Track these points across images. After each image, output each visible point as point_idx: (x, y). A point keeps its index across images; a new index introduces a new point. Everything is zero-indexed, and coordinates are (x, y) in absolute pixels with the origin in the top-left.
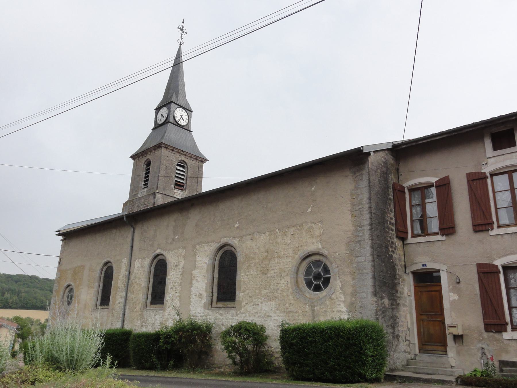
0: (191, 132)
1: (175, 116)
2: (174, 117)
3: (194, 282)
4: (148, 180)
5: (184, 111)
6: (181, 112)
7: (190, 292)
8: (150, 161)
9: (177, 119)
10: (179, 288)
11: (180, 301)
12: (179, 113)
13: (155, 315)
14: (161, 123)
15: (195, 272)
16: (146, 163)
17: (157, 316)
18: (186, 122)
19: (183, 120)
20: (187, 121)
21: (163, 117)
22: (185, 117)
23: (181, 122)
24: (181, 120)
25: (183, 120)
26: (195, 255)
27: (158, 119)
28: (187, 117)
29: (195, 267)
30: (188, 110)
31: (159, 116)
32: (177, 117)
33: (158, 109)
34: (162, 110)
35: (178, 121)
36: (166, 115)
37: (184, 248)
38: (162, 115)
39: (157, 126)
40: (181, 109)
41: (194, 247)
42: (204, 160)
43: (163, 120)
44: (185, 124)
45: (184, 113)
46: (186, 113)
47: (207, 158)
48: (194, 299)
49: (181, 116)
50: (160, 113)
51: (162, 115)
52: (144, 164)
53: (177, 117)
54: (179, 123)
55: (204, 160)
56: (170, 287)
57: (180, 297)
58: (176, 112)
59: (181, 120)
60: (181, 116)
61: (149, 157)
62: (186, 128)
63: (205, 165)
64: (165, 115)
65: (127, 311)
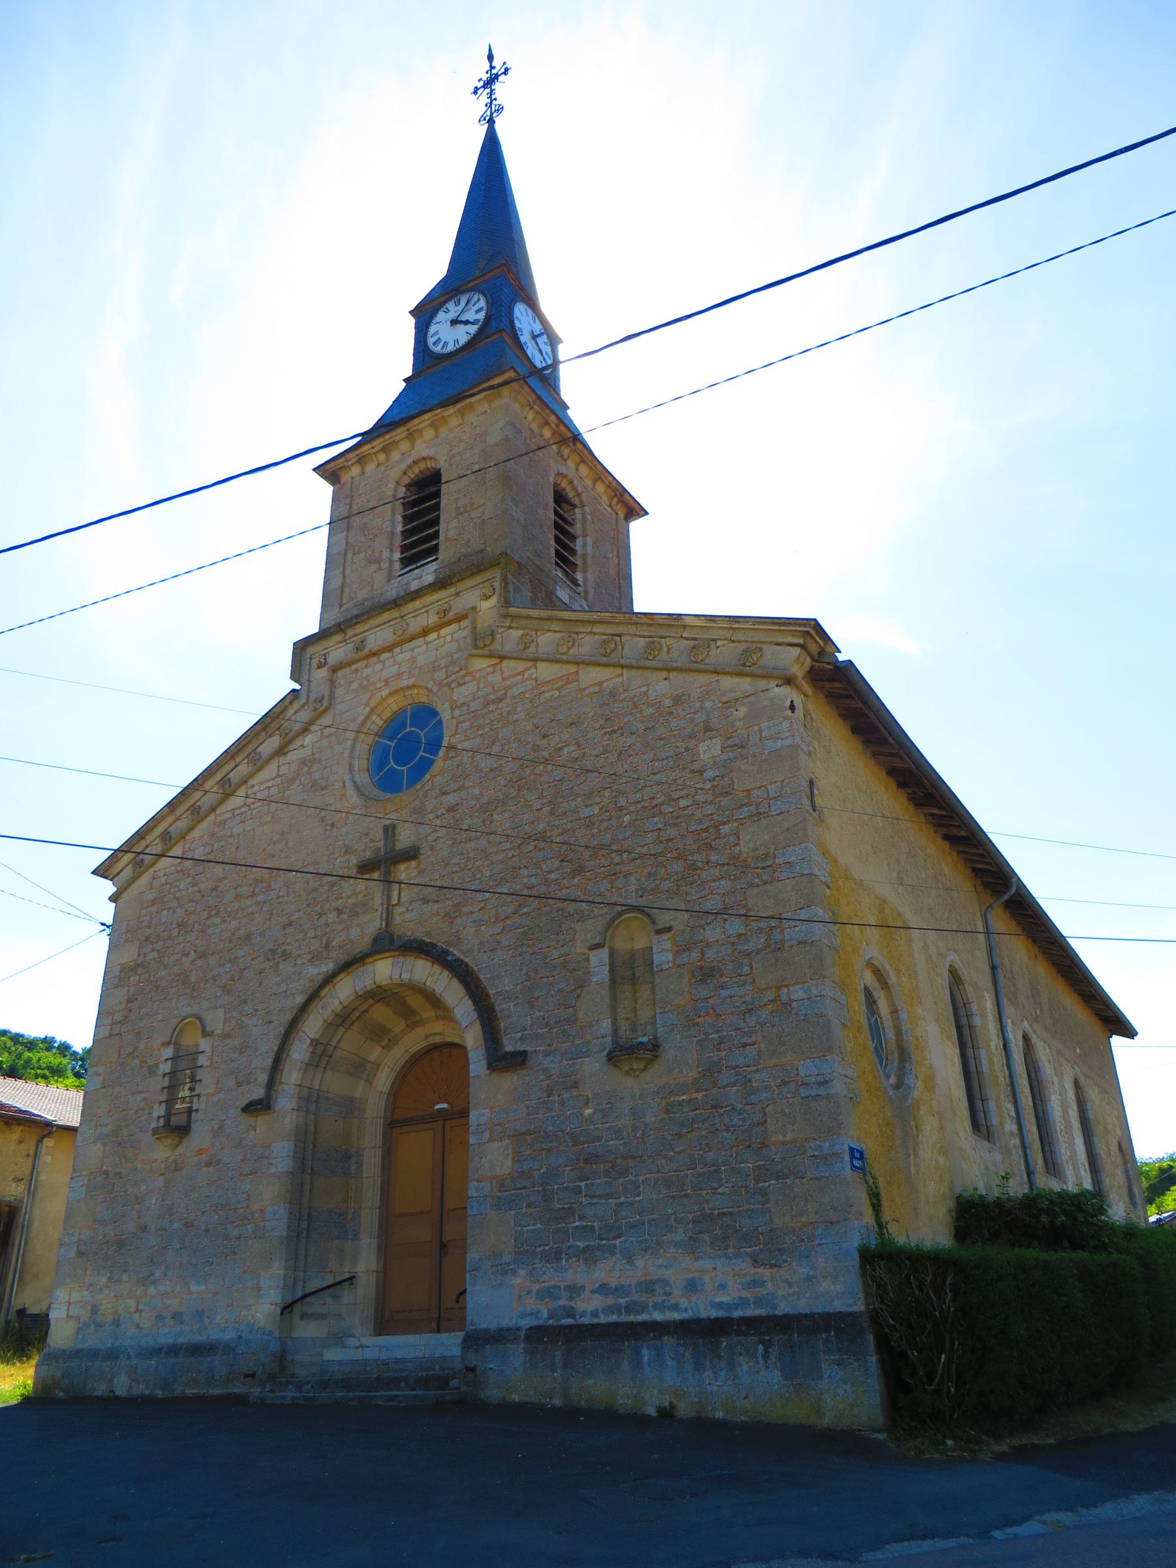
33: (424, 313)
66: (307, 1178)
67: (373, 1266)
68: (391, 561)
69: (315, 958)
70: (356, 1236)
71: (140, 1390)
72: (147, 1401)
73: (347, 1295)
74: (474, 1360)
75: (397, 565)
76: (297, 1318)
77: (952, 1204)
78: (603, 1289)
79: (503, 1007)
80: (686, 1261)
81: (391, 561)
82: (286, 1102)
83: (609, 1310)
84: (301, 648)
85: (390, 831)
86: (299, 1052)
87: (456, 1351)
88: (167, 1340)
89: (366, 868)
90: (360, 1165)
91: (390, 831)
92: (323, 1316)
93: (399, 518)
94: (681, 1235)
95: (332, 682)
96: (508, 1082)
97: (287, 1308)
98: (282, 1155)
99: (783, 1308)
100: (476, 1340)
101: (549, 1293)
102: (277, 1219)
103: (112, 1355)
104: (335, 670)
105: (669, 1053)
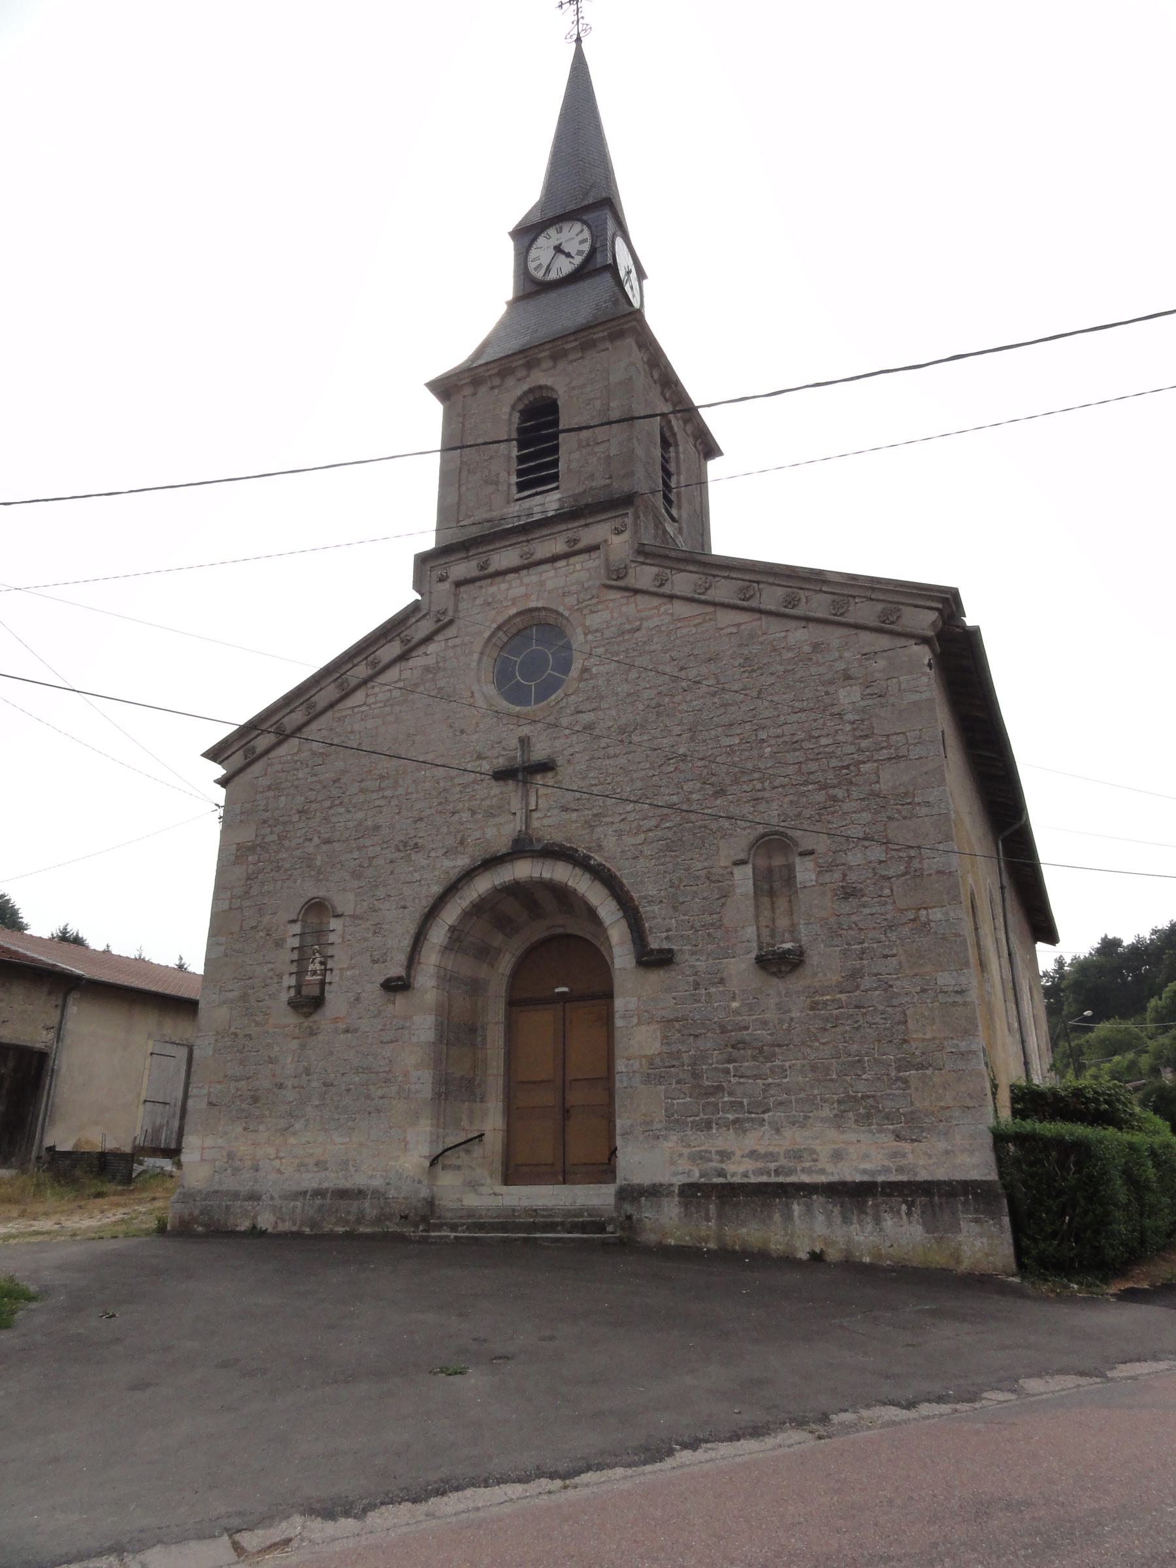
16: (521, 406)
52: (513, 408)
68: (509, 485)
73: (477, 1151)
75: (514, 489)
78: (753, 1154)
80: (832, 1134)
81: (509, 485)
82: (426, 980)
83: (761, 1172)
92: (459, 1168)
98: (424, 1028)
99: (923, 1176)
102: (423, 1082)
103: (254, 1197)
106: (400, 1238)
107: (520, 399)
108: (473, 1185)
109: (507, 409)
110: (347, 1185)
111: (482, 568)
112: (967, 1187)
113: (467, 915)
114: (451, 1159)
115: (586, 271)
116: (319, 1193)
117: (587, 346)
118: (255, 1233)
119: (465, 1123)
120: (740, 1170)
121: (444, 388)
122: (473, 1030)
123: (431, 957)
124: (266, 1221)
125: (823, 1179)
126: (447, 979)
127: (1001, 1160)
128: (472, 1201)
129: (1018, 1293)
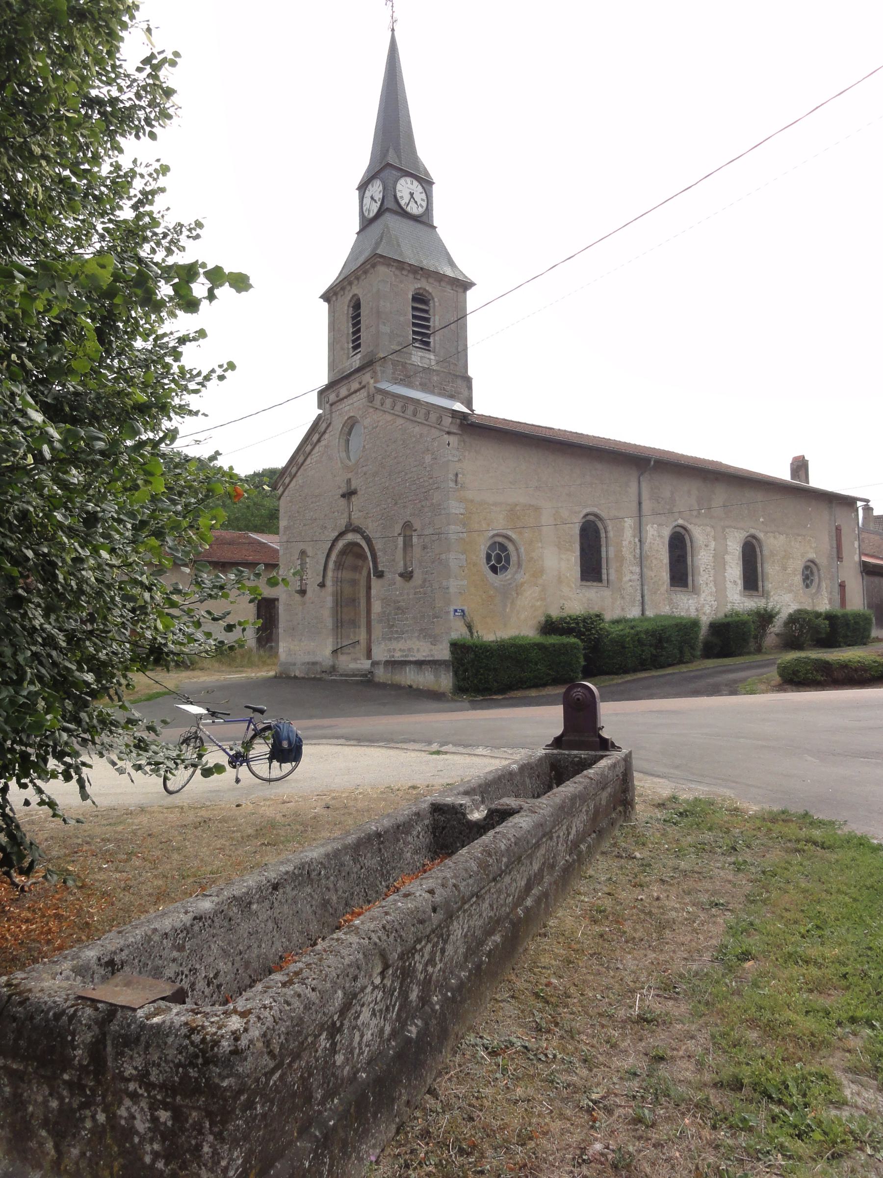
0: (435, 228)
1: (399, 195)
2: (395, 196)
3: (727, 567)
4: (359, 338)
5: (415, 183)
6: (409, 185)
7: (725, 577)
8: (359, 300)
9: (403, 203)
10: (712, 572)
11: (715, 586)
12: (405, 188)
13: (688, 600)
14: (372, 215)
15: (728, 558)
16: (352, 304)
17: (690, 601)
18: (422, 207)
19: (416, 202)
20: (424, 204)
21: (376, 202)
22: (420, 196)
23: (412, 208)
24: (412, 204)
25: (416, 202)
26: (725, 539)
27: (364, 209)
28: (424, 196)
29: (726, 552)
30: (426, 183)
31: (367, 201)
32: (402, 197)
33: (363, 187)
34: (370, 186)
35: (405, 207)
36: (381, 196)
37: (712, 527)
38: (372, 198)
39: (366, 223)
40: (409, 180)
41: (724, 528)
42: (465, 285)
43: (375, 208)
44: (421, 210)
45: (416, 187)
46: (420, 186)
47: (474, 280)
48: (729, 585)
49: (412, 194)
50: (368, 194)
51: (372, 198)
52: (348, 306)
53: (402, 197)
54: (409, 209)
55: (465, 285)
56: (702, 569)
57: (715, 581)
58: (399, 187)
59: (412, 204)
60: (412, 194)
61: (355, 290)
62: (424, 220)
63: (469, 293)
64: (378, 196)
65: (646, 592)
66: (339, 609)
67: (365, 637)
68: (348, 349)
69: (333, 530)
70: (359, 627)
71: (302, 675)
72: (303, 678)
73: (358, 647)
74: (373, 670)
75: (351, 350)
76: (339, 654)
77: (543, 619)
78: (400, 650)
79: (379, 554)
80: (417, 642)
81: (348, 349)
82: (329, 583)
83: (402, 656)
84: (322, 393)
85: (349, 481)
86: (331, 565)
87: (369, 666)
88: (307, 660)
89: (343, 496)
90: (359, 603)
91: (349, 481)
92: (349, 654)
93: (350, 325)
94: (416, 634)
95: (331, 413)
96: (380, 581)
97: (335, 652)
98: (329, 601)
99: (436, 658)
100: (375, 664)
101: (389, 651)
102: (329, 622)
103: (295, 664)
104: (331, 405)
105: (415, 575)
106: (320, 679)
107: (350, 301)
108: (355, 660)
109: (346, 308)
110: (314, 660)
111: (349, 390)
112: (445, 661)
113: (338, 556)
114: (346, 650)
115: (400, 210)
116: (308, 663)
117: (366, 272)
118: (296, 677)
119: (352, 637)
120: (398, 656)
121: (327, 297)
122: (354, 600)
123: (330, 574)
124: (297, 674)
125: (414, 659)
126: (337, 581)
127: (452, 653)
128: (353, 666)
129: (453, 700)
